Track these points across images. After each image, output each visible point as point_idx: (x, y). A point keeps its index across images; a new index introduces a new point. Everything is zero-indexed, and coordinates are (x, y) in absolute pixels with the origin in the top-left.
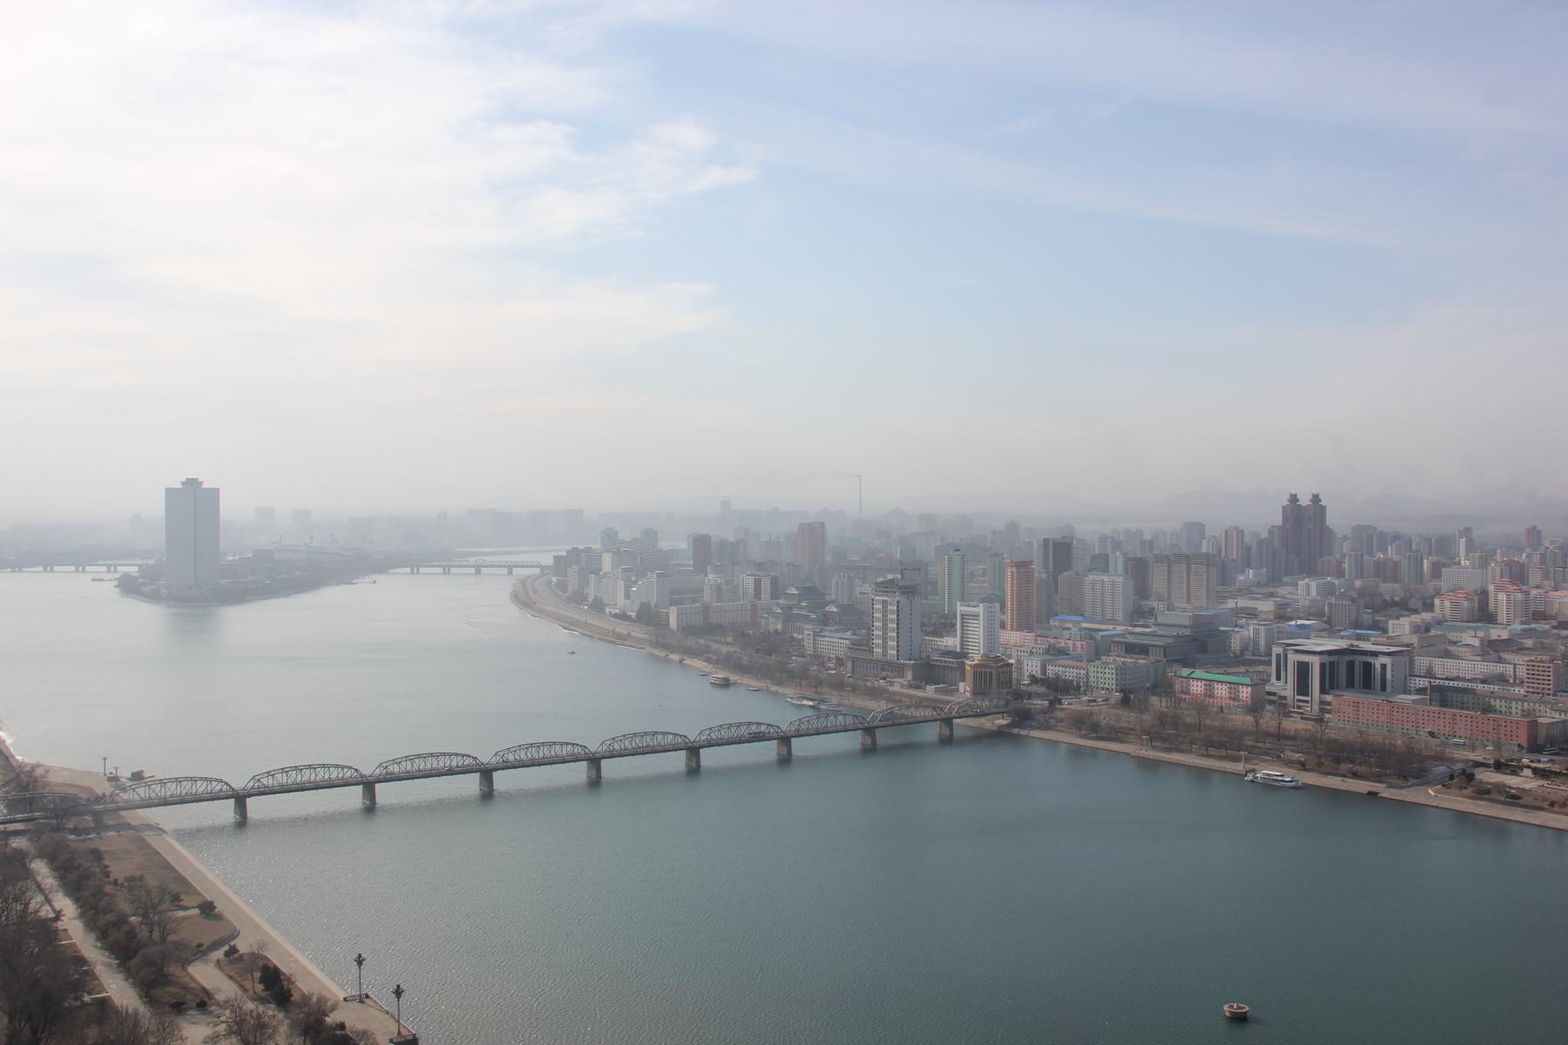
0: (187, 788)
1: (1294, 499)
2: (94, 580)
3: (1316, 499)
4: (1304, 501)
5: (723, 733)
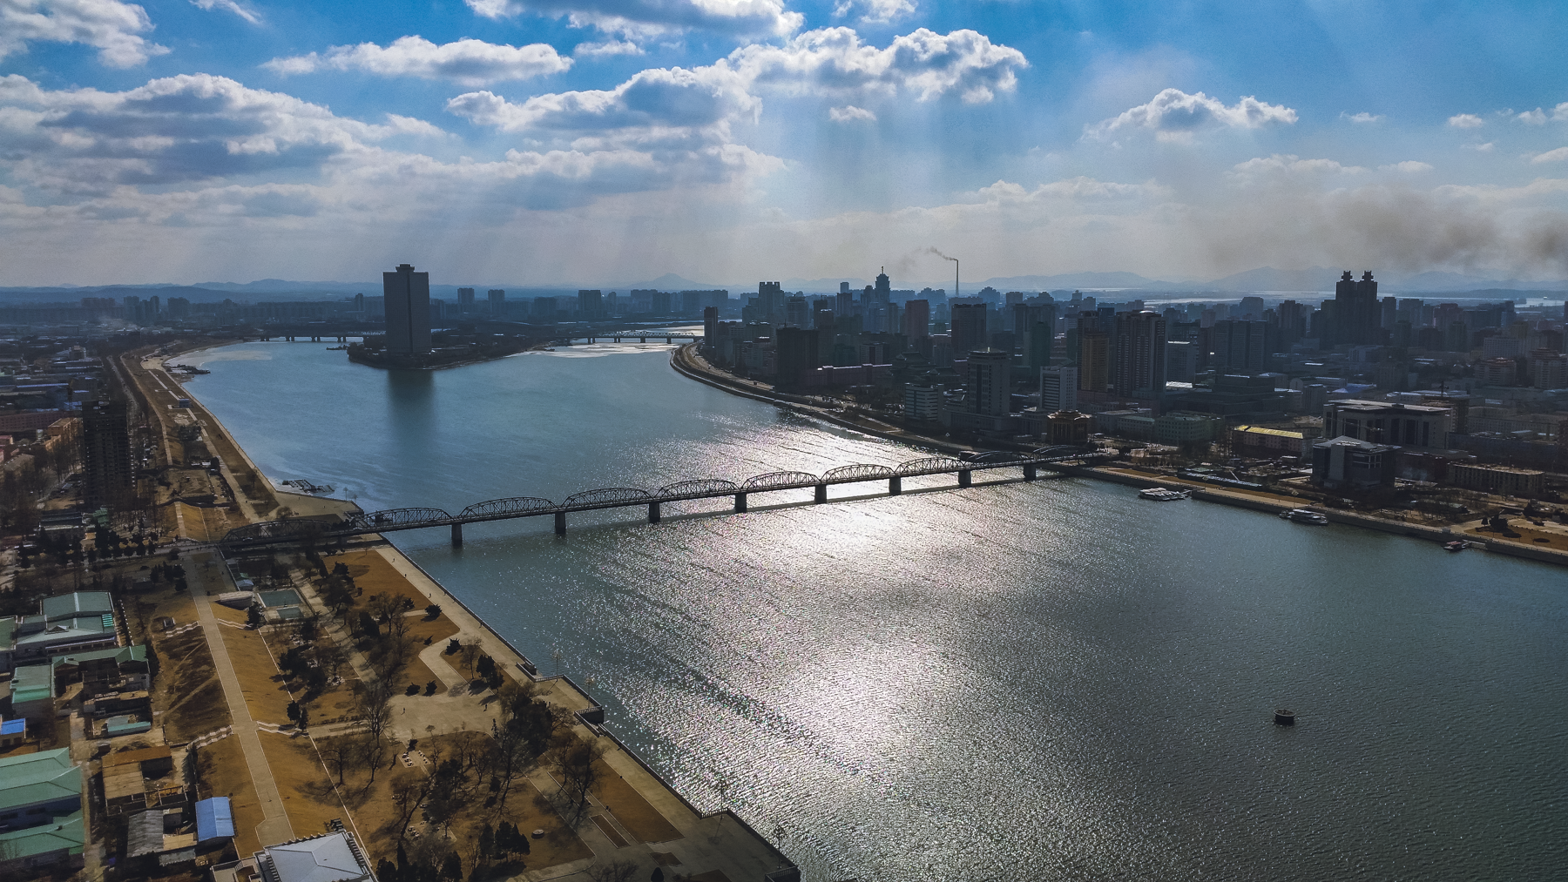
0: (510, 506)
1: (1347, 275)
2: (328, 349)
3: (1368, 275)
4: (1357, 278)
5: (845, 473)
